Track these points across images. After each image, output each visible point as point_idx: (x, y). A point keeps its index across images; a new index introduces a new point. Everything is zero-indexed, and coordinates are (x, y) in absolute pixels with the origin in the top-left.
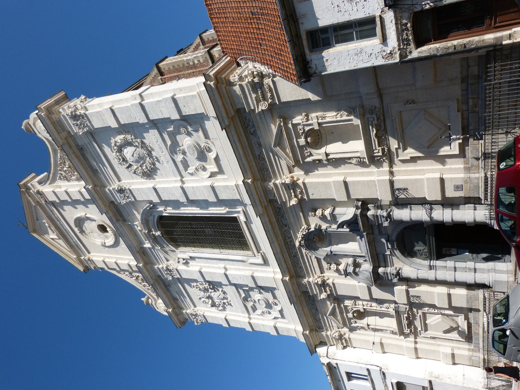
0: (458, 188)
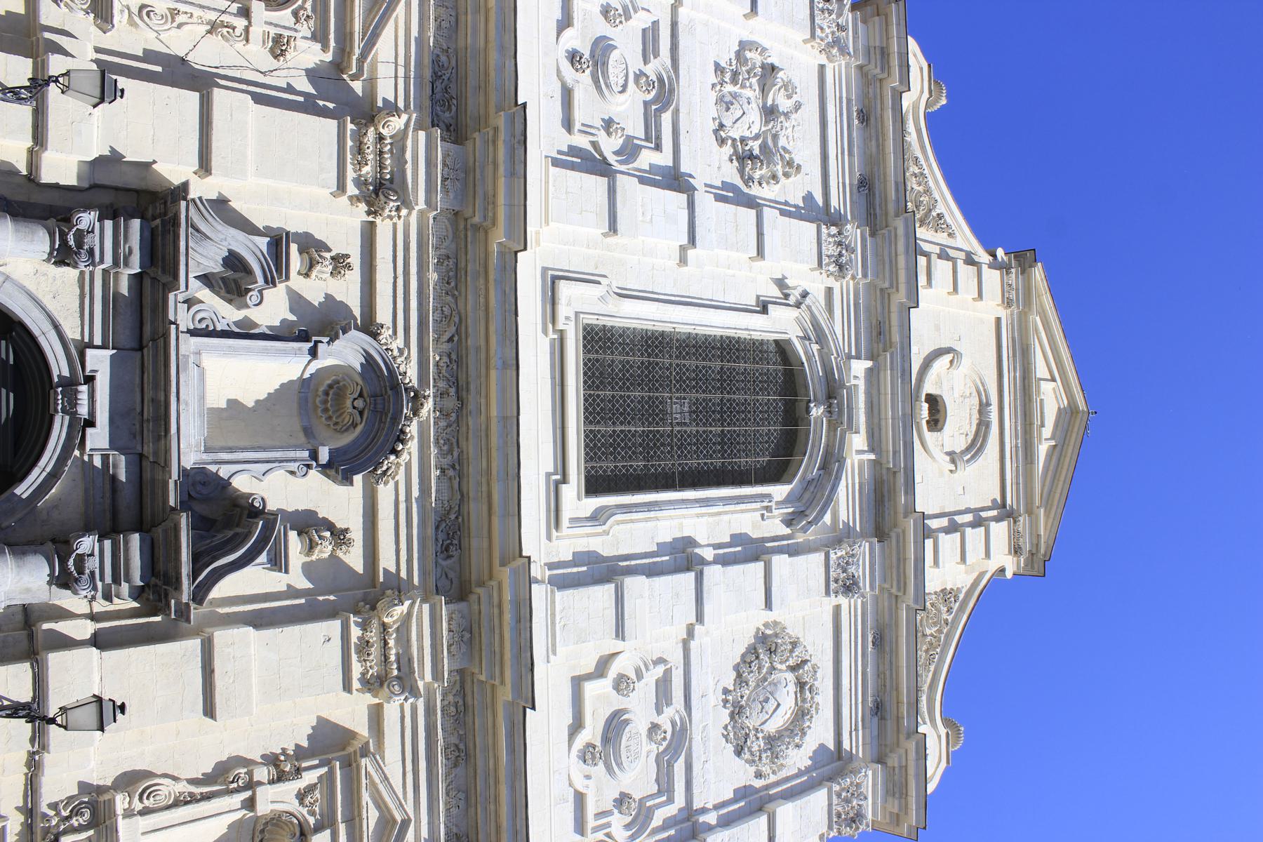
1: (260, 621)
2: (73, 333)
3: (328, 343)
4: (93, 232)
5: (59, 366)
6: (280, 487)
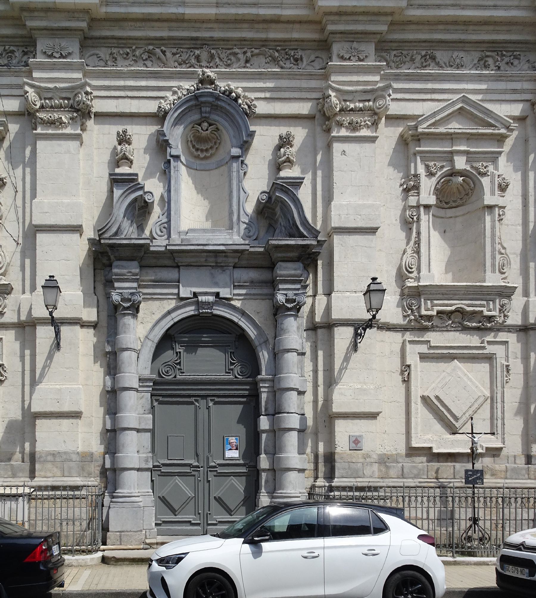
0: (356, 443)
1: (328, 199)
2: (173, 304)
3: (171, 148)
4: (121, 293)
6: (255, 182)
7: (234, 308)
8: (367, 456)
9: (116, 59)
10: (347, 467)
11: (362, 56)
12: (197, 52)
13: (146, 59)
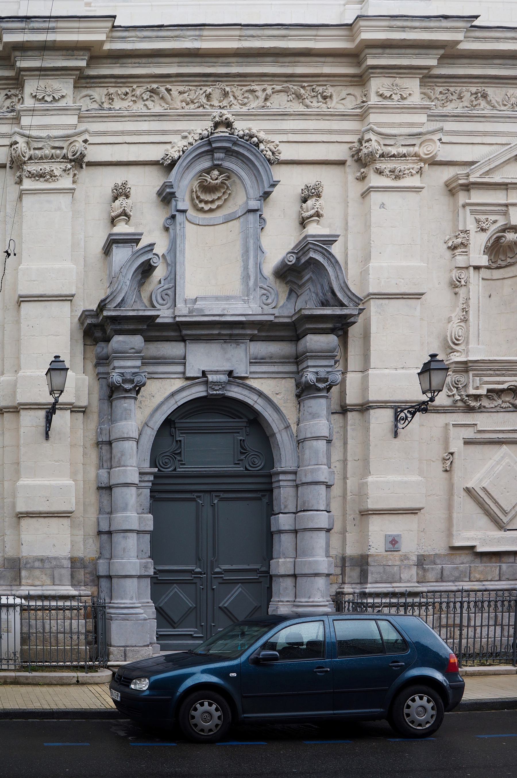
0: (393, 543)
2: (179, 384)
4: (122, 373)
5: (198, 392)
7: (251, 389)
8: (406, 557)
9: (113, 100)
10: (382, 571)
11: (406, 94)
12: (209, 90)
13: (147, 100)
